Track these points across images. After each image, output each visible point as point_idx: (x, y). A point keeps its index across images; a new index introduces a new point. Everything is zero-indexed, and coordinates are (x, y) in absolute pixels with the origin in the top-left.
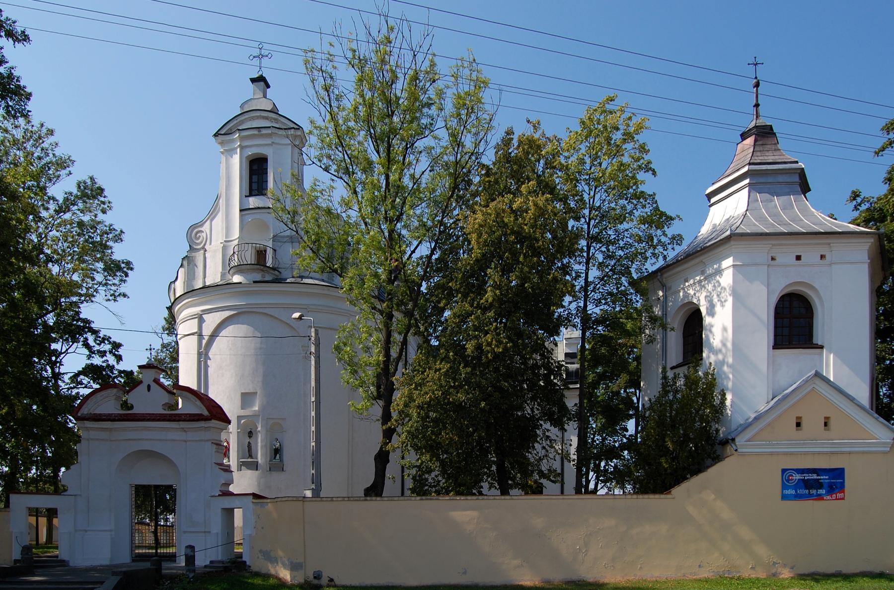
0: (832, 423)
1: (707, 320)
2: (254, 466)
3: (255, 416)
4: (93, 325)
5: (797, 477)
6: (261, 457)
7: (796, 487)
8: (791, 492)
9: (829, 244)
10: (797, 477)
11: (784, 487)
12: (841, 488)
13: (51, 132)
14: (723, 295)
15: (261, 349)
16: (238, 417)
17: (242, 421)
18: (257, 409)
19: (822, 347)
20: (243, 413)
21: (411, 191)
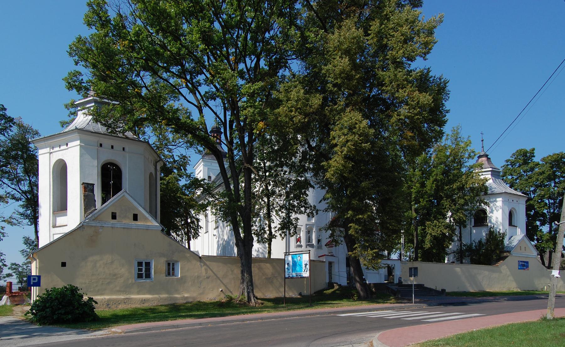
0: (125, 149)
1: (489, 215)
2: (312, 246)
3: (313, 225)
4: (553, 253)
5: (521, 263)
6: (314, 242)
7: (521, 266)
8: (520, 267)
9: (519, 198)
10: (521, 263)
11: (519, 266)
12: (527, 267)
13: (87, 3)
14: (497, 208)
15: (315, 196)
16: (306, 224)
17: (308, 227)
18: (314, 221)
19: (517, 227)
20: (308, 223)
21: (178, 90)
